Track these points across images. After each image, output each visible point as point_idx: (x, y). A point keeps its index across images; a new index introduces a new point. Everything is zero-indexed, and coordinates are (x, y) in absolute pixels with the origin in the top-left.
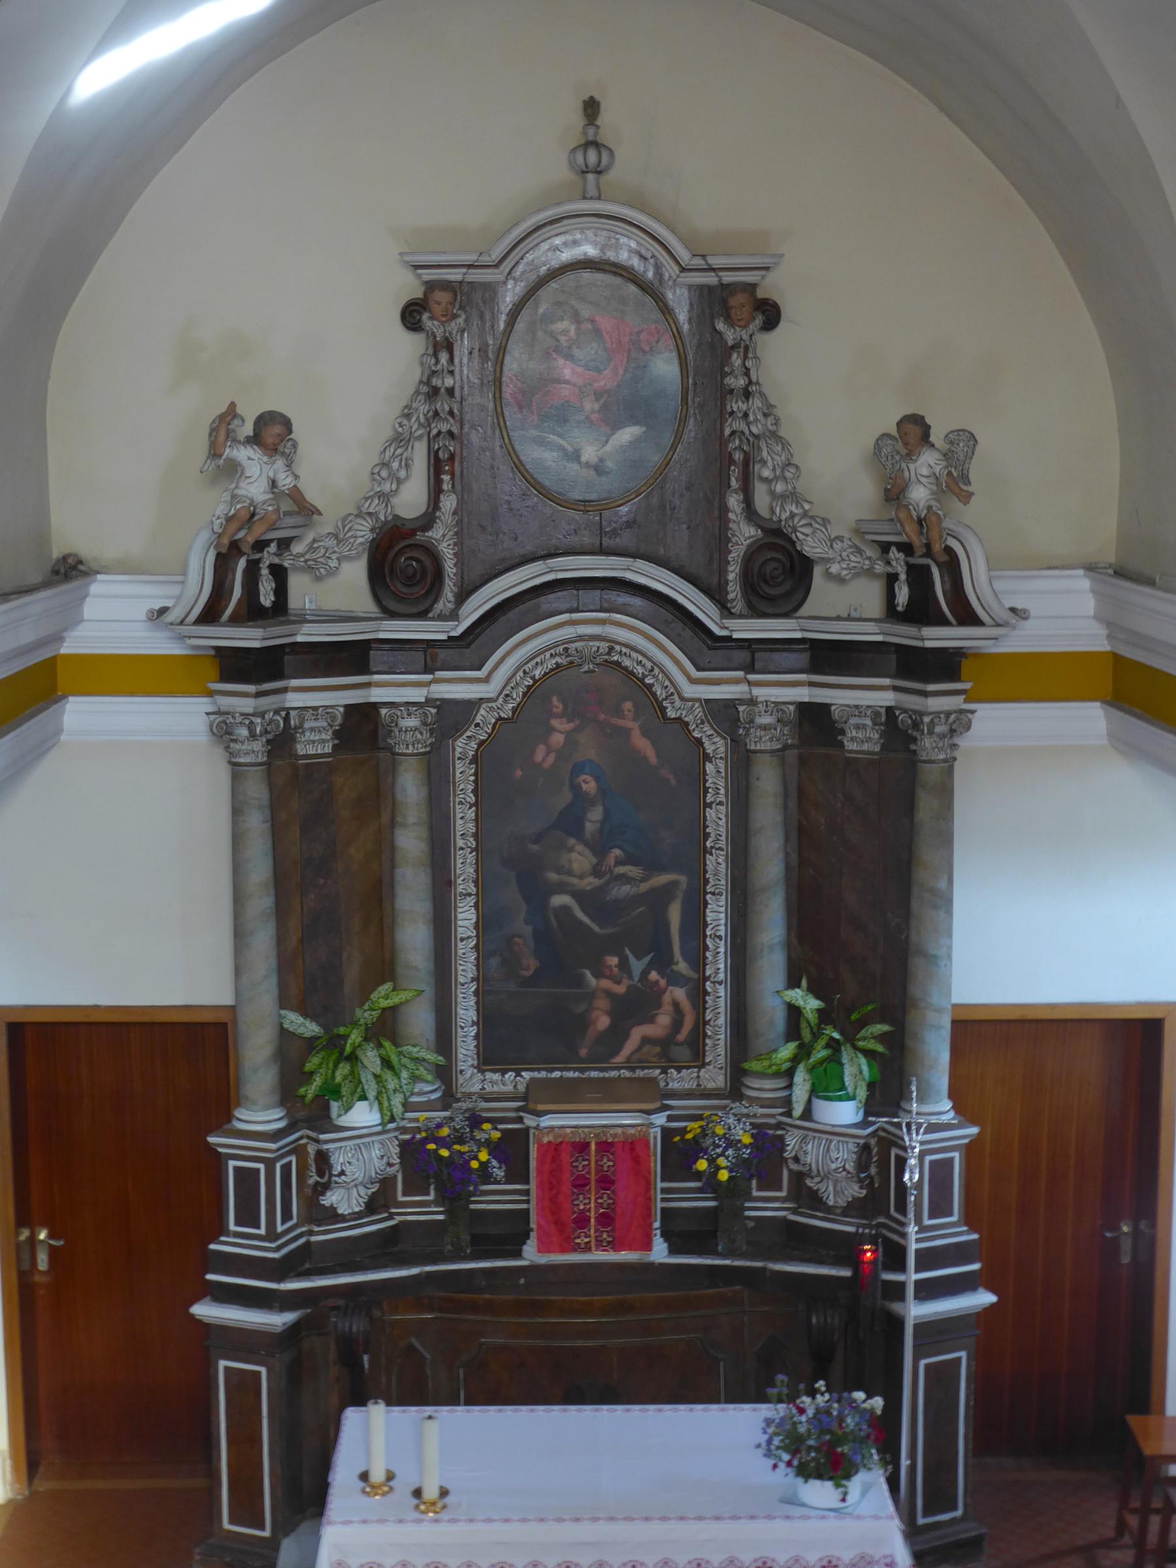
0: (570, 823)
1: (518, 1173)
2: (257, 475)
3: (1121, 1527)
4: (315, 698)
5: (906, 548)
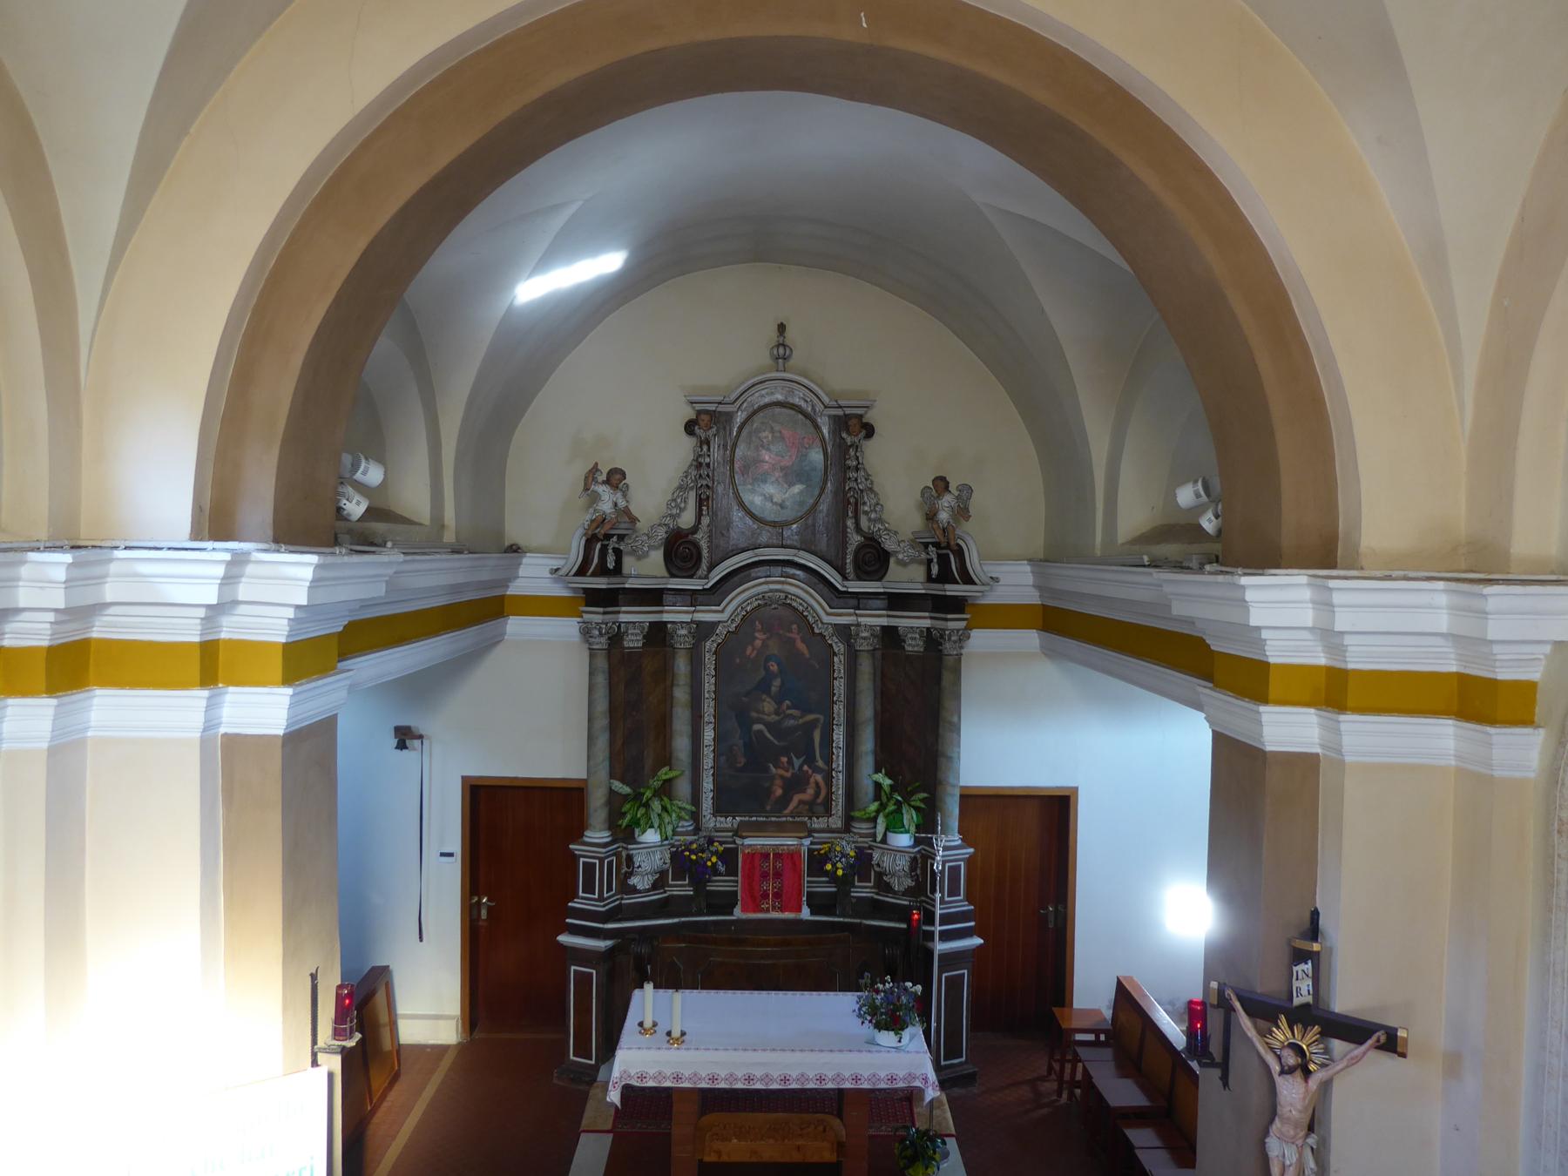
0: (763, 687)
1: (732, 871)
2: (607, 500)
3: (1050, 1069)
4: (634, 617)
5: (937, 545)
